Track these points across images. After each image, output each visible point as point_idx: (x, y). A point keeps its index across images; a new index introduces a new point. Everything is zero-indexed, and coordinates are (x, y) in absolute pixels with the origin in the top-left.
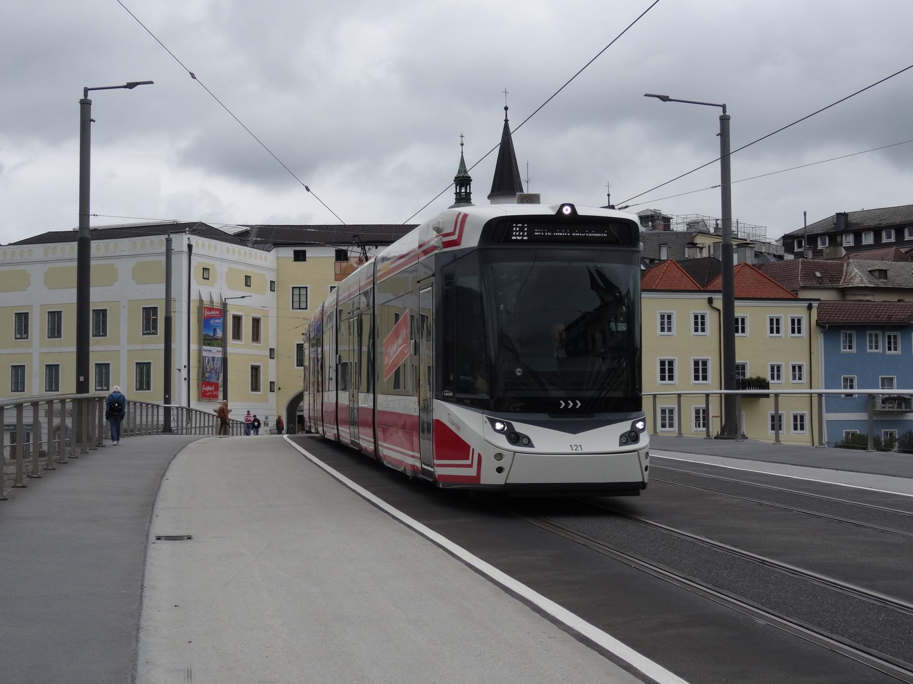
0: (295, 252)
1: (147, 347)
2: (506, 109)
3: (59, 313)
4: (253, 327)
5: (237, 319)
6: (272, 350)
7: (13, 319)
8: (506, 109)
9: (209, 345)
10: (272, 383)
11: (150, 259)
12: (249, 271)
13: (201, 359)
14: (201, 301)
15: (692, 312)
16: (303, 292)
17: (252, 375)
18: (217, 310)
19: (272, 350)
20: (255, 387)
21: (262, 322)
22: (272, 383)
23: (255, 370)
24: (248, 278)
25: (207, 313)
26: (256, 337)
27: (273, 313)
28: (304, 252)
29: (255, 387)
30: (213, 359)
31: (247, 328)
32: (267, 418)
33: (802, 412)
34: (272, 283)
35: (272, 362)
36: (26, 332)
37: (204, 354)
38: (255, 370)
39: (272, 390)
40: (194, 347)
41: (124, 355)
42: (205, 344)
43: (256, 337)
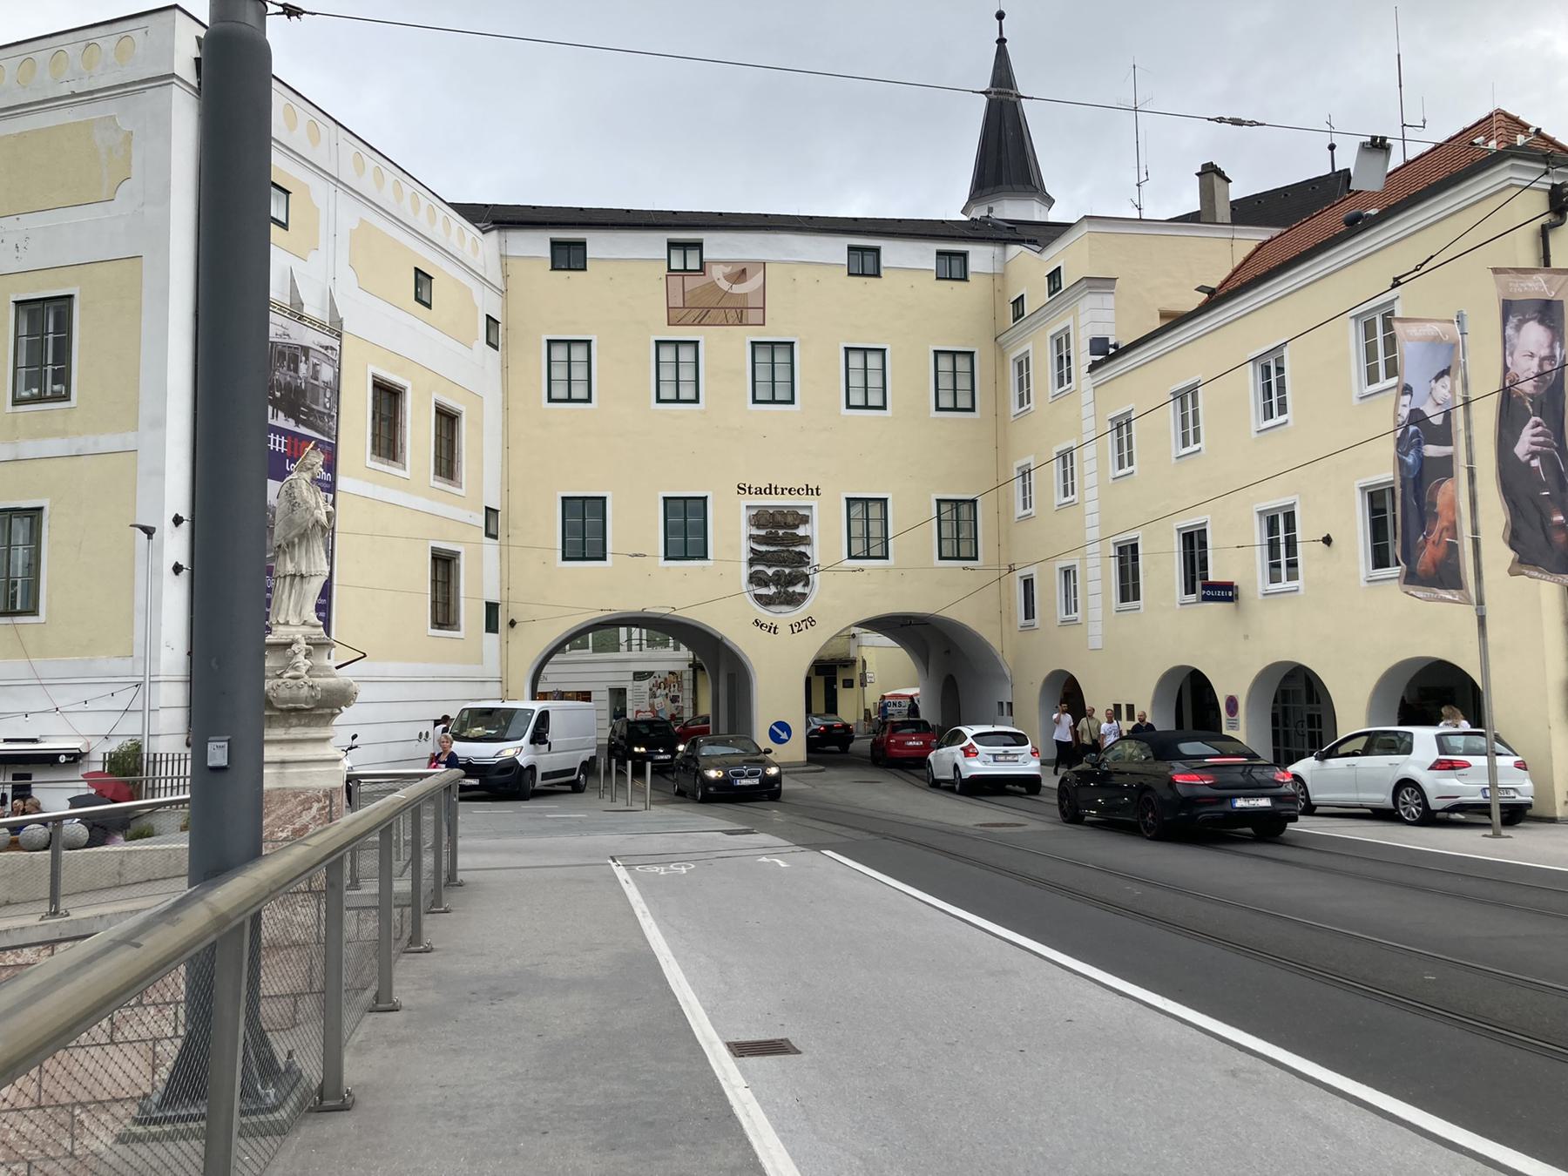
0: (555, 244)
1: (29, 448)
2: (1000, 16)
4: (438, 436)
5: (387, 397)
6: (490, 512)
7: (1176, 545)
8: (1000, 16)
11: (65, 116)
12: (431, 262)
15: (1208, 517)
16: (579, 353)
17: (434, 581)
19: (490, 512)
20: (444, 615)
22: (492, 609)
23: (444, 563)
24: (422, 278)
26: (446, 465)
28: (582, 244)
33: (744, 515)
35: (491, 546)
36: (63, 377)
38: (444, 563)
39: (492, 626)
43: (446, 465)
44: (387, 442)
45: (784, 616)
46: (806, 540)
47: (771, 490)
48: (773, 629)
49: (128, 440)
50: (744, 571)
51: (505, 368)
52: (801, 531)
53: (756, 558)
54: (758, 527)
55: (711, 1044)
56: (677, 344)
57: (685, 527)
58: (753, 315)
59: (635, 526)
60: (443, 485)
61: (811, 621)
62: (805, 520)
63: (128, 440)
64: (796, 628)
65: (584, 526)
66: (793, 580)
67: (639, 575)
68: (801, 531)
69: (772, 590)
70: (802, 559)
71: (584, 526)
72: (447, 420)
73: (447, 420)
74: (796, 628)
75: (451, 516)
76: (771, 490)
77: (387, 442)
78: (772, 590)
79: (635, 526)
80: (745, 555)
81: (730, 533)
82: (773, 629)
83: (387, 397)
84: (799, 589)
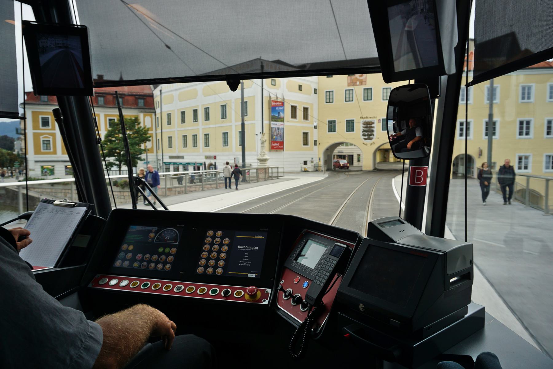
3: (304, 144)
5: (294, 109)
9: (275, 121)
10: (315, 141)
13: (271, 129)
14: (270, 97)
18: (280, 102)
20: (306, 143)
21: (309, 134)
22: (315, 141)
23: (306, 135)
25: (274, 104)
26: (306, 117)
27: (315, 107)
29: (306, 143)
30: (278, 129)
31: (300, 113)
32: (312, 159)
34: (315, 90)
37: (272, 126)
38: (306, 135)
39: (315, 144)
40: (266, 122)
41: (234, 127)
42: (272, 121)
43: (306, 117)
44: (294, 115)
45: (368, 142)
46: (373, 127)
47: (367, 118)
48: (366, 145)
49: (253, 122)
50: (361, 133)
51: (319, 97)
52: (373, 125)
53: (364, 131)
54: (364, 124)
55: (46, 109)
56: (349, 90)
57: (350, 125)
58: (364, 83)
59: (341, 127)
60: (305, 121)
61: (374, 143)
62: (373, 123)
63: (253, 122)
64: (371, 144)
65: (332, 126)
66: (371, 135)
67: (341, 133)
68: (373, 125)
69: (366, 137)
70: (373, 131)
71: (332, 126)
72: (306, 110)
73: (306, 110)
74: (371, 144)
75: (306, 126)
76: (367, 118)
77: (294, 115)
78: (366, 137)
79: (341, 127)
80: (362, 130)
81: (359, 127)
82: (366, 145)
83: (294, 109)
84: (372, 137)
